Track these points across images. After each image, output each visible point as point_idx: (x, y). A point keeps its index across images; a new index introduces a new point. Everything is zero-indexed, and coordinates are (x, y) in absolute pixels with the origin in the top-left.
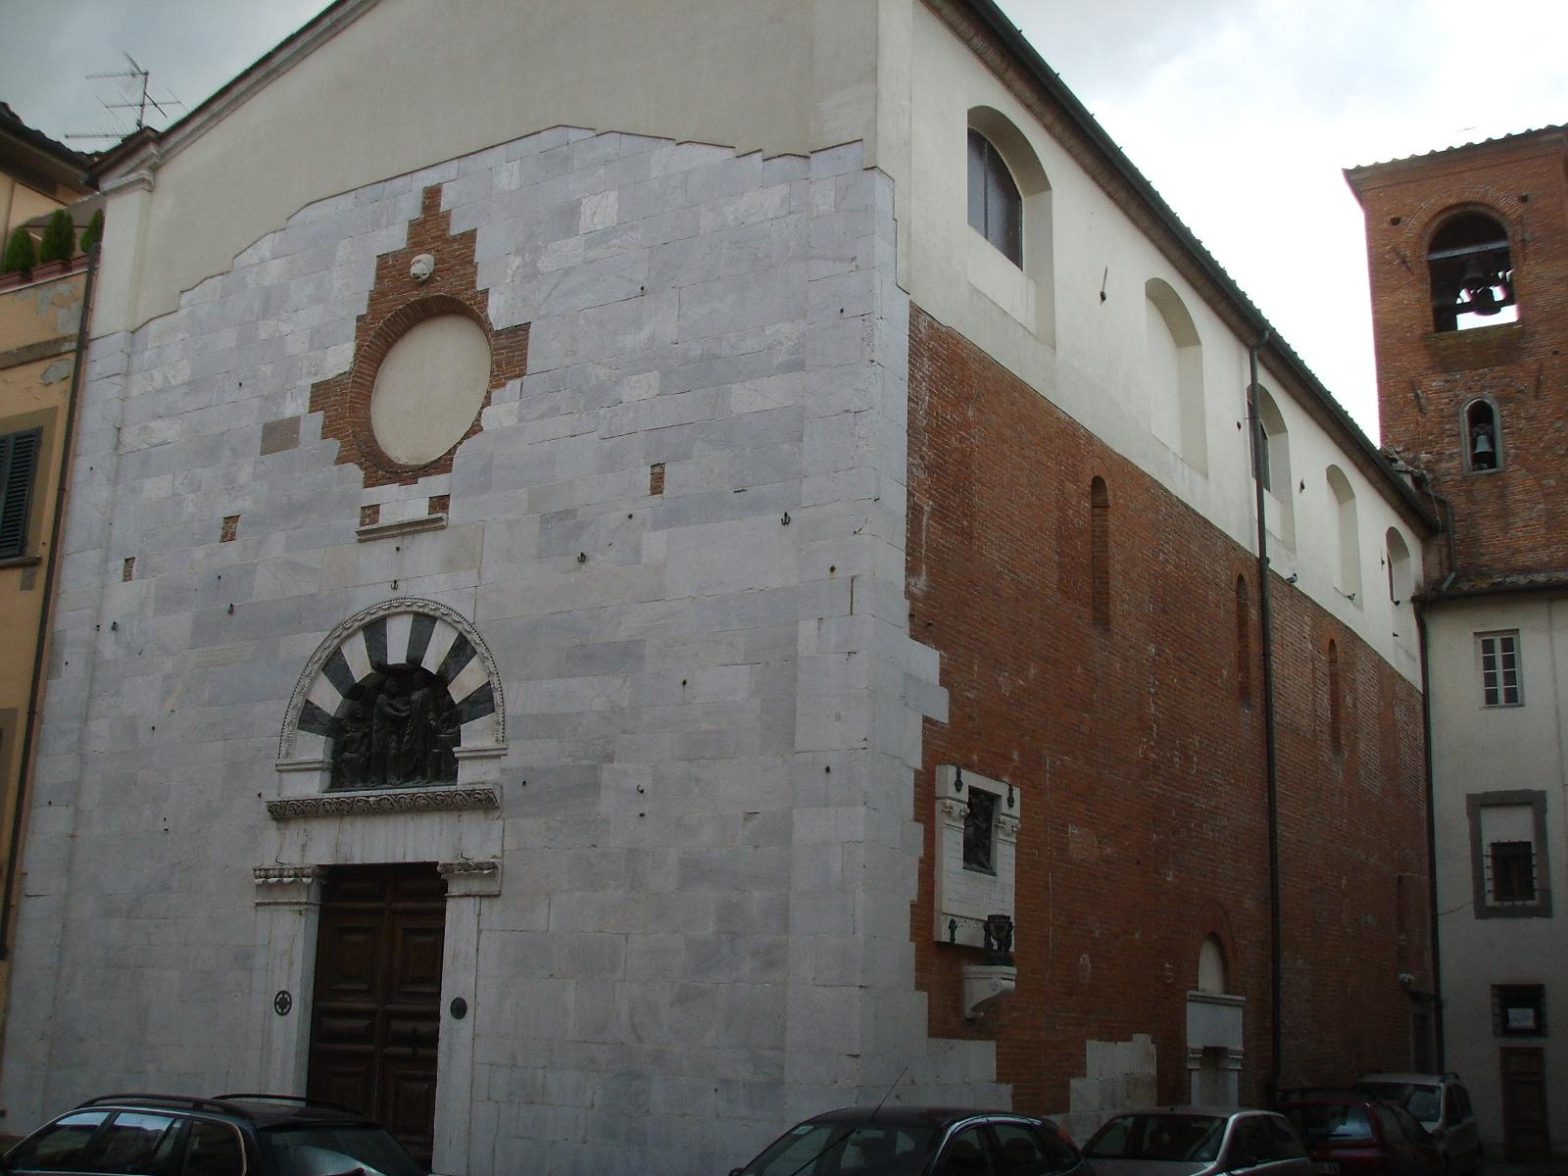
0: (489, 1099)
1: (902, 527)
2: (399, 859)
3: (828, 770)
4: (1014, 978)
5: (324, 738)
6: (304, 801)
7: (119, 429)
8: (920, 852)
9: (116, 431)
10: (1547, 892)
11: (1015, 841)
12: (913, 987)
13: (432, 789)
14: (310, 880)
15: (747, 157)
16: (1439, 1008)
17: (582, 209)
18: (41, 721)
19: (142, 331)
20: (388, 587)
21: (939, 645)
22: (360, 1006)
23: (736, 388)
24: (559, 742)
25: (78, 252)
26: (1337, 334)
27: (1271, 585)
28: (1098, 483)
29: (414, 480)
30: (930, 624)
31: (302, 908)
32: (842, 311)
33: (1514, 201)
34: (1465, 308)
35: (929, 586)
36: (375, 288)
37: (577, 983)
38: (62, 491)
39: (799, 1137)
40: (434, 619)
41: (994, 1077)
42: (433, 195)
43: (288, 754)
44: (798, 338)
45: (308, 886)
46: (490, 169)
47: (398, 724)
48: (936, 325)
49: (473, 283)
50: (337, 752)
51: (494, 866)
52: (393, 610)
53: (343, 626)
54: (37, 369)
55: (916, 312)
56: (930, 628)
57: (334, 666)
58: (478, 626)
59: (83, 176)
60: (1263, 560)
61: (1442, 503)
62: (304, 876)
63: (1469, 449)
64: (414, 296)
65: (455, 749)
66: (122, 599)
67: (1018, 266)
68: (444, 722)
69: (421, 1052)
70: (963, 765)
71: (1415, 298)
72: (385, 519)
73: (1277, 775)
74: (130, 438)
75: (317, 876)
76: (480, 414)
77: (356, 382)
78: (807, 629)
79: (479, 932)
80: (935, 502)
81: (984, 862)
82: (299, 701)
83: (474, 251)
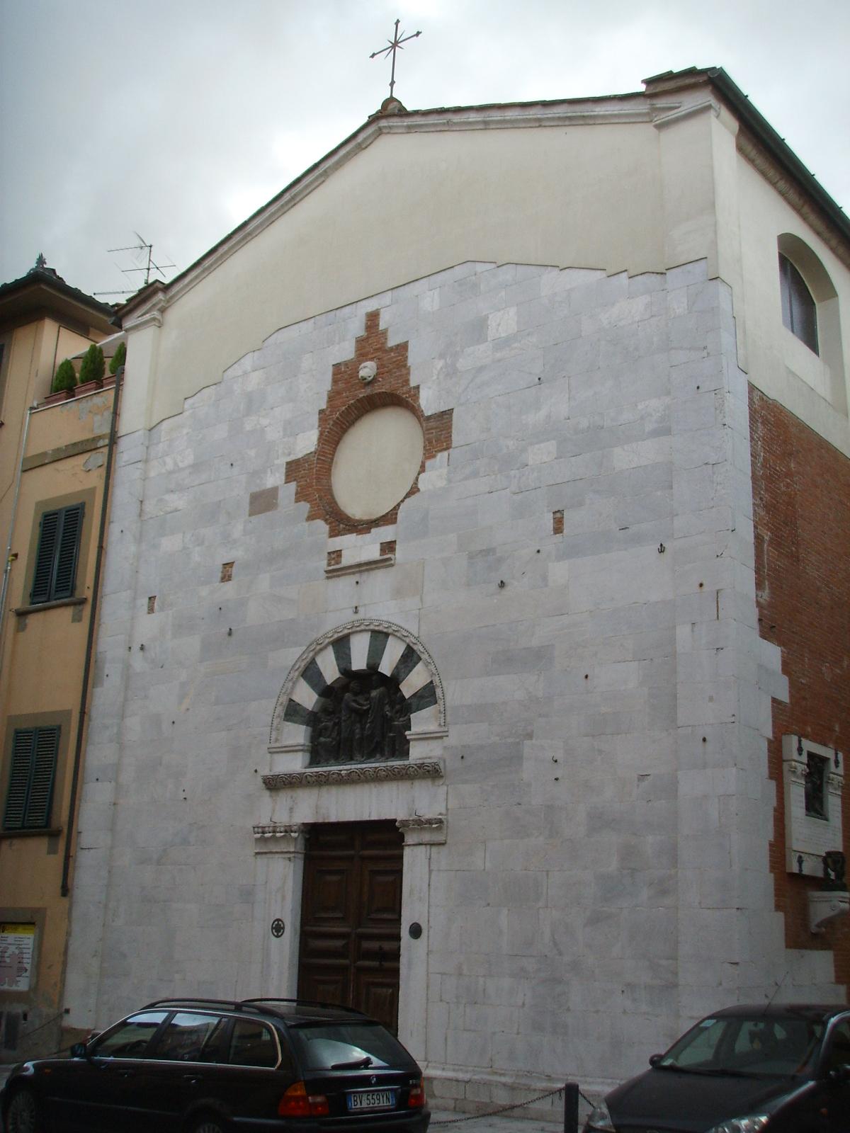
0: (441, 1000)
1: (751, 551)
2: (366, 817)
3: (704, 740)
4: (848, 900)
5: (305, 727)
6: (291, 774)
7: (141, 502)
8: (774, 803)
9: (140, 503)
11: (840, 794)
12: (773, 909)
13: (390, 764)
14: (296, 835)
15: (616, 276)
17: (489, 322)
18: (90, 720)
20: (351, 611)
21: (780, 643)
22: (336, 930)
23: (617, 451)
24: (490, 725)
25: (108, 374)
29: (368, 530)
30: (774, 627)
31: (292, 855)
32: (698, 388)
35: (772, 598)
36: (332, 389)
37: (509, 910)
38: (101, 548)
39: (706, 1028)
40: (387, 635)
41: (833, 980)
42: (373, 318)
43: (277, 740)
44: (664, 411)
45: (296, 839)
46: (417, 296)
47: (362, 715)
48: (764, 397)
49: (407, 381)
50: (314, 738)
51: (440, 821)
52: (354, 629)
53: (317, 642)
54: (81, 460)
55: (752, 388)
56: (774, 630)
57: (310, 673)
58: (423, 639)
59: (110, 320)
62: (292, 832)
64: (362, 393)
65: (407, 733)
66: (147, 627)
67: (816, 353)
68: (397, 712)
69: (387, 964)
70: (801, 735)
72: (346, 560)
74: (150, 507)
75: (302, 832)
76: (417, 479)
77: (320, 459)
78: (683, 632)
79: (430, 871)
80: (772, 533)
81: (820, 810)
82: (284, 699)
83: (407, 357)
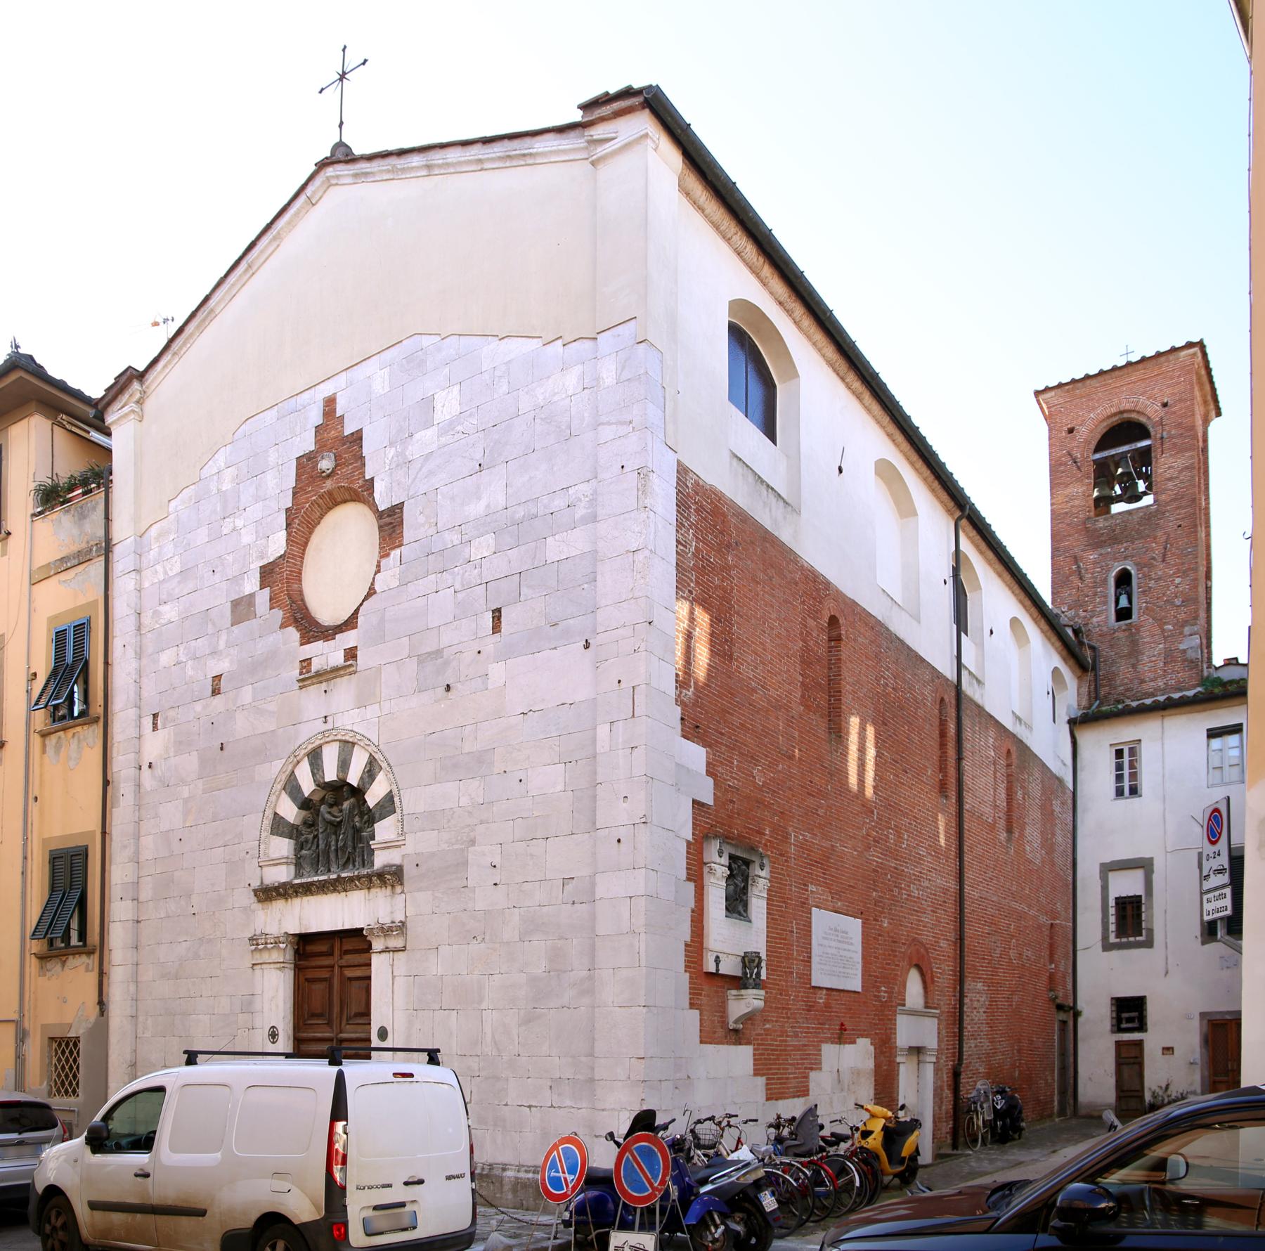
3: (619, 841)
8: (692, 905)
10: (1150, 931)
16: (1077, 1014)
19: (146, 535)
26: (1025, 519)
27: (964, 701)
28: (833, 621)
33: (1158, 407)
34: (1119, 499)
40: (354, 744)
41: (752, 1072)
42: (330, 402)
50: (300, 847)
55: (682, 471)
60: (958, 687)
61: (1093, 648)
63: (1113, 605)
66: (155, 745)
71: (1084, 491)
73: (966, 848)
74: (147, 620)
78: (603, 731)
79: (393, 977)
82: (269, 814)
